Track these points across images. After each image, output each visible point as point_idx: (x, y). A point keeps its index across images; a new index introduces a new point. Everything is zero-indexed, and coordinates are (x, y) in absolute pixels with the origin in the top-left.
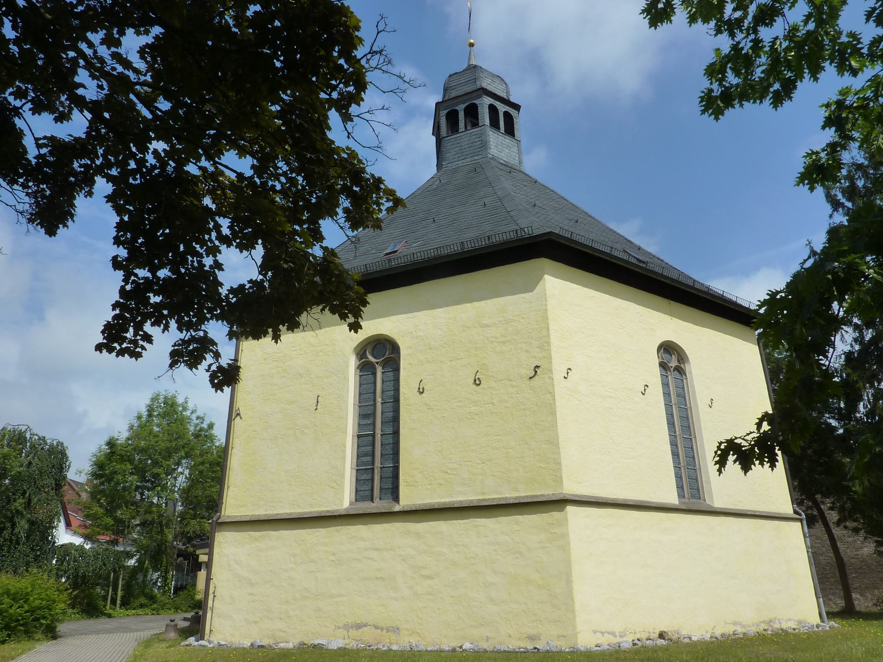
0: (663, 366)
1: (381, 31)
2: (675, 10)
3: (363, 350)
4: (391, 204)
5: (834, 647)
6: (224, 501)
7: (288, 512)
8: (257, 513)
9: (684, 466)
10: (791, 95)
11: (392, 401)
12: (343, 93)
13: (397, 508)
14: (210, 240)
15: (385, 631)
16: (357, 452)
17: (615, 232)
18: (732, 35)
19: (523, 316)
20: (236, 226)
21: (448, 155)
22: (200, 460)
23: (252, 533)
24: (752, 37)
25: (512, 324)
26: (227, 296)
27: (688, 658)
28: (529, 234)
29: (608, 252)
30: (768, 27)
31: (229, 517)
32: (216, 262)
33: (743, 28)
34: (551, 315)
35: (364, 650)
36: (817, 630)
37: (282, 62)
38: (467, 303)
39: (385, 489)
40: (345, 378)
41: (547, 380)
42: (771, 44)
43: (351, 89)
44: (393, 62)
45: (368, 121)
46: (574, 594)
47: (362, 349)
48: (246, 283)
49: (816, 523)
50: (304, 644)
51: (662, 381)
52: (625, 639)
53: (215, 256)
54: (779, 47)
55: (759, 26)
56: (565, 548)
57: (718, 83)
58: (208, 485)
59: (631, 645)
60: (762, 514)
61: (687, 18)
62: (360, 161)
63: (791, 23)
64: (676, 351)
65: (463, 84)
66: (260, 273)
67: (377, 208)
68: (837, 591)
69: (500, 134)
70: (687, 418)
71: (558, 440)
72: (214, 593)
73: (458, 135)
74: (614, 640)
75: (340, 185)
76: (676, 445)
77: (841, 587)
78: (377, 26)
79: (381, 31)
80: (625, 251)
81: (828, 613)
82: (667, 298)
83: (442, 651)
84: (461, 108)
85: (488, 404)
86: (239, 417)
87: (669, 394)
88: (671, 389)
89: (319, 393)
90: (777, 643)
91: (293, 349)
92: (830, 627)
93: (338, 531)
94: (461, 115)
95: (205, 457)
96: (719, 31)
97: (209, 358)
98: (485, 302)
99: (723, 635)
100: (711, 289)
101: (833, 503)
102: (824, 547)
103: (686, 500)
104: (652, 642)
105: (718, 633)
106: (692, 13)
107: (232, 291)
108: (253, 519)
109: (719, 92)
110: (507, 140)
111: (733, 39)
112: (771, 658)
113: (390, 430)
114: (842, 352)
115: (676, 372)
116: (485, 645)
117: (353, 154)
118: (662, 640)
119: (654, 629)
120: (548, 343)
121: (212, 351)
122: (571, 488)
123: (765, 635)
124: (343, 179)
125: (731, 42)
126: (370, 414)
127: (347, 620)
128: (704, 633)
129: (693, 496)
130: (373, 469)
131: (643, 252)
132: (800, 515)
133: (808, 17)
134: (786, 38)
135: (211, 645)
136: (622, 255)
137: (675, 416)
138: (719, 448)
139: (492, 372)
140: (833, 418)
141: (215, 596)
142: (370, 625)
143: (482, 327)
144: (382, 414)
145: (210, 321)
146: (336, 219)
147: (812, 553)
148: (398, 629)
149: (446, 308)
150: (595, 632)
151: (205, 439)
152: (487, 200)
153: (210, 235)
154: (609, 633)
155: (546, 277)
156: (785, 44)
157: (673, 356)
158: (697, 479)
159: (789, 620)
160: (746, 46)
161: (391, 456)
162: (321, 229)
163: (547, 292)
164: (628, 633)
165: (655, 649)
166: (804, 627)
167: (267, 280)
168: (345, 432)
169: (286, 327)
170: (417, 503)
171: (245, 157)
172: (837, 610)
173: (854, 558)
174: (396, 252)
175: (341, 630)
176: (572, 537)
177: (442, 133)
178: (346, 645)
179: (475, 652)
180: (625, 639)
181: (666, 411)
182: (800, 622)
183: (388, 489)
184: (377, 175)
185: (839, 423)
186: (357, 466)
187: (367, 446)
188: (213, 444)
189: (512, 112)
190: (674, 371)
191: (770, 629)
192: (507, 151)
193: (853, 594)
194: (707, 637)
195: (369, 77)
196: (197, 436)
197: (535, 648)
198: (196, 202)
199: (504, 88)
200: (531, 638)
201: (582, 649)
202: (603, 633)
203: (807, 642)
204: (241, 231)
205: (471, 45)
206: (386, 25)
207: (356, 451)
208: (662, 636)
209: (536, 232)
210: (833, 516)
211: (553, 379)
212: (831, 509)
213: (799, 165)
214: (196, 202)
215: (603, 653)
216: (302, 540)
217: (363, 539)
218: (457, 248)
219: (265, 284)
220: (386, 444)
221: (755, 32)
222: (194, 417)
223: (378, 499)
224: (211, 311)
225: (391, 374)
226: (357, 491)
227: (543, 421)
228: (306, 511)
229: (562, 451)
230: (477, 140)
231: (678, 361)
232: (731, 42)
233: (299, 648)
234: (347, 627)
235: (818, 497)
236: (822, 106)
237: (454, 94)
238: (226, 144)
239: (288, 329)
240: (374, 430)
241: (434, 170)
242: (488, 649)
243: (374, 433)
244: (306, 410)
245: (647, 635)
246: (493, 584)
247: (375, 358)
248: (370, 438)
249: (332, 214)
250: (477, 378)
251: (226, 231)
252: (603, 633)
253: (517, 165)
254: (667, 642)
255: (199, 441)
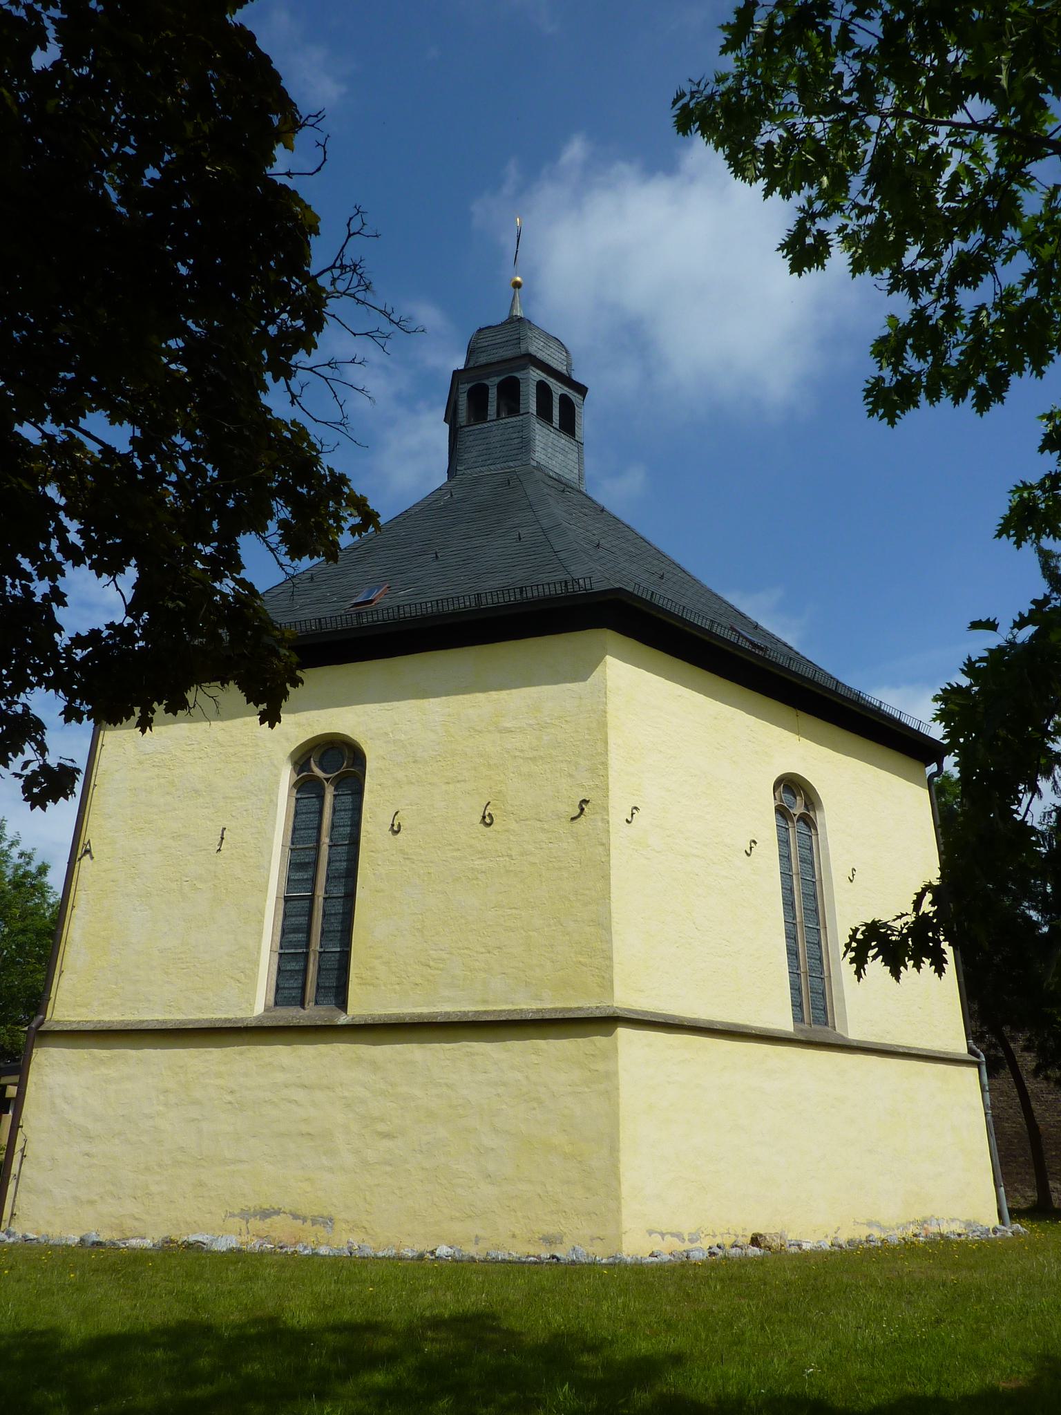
0: (782, 812)
1: (354, 234)
2: (831, 249)
3: (306, 759)
4: (358, 520)
5: (1018, 1262)
6: (52, 995)
7: (161, 1018)
8: (106, 1018)
9: (806, 972)
10: (1003, 394)
11: (346, 842)
12: (287, 328)
13: (343, 1020)
14: (47, 551)
15: (309, 1222)
16: (283, 925)
17: (720, 598)
18: (915, 295)
19: (568, 719)
20: (93, 531)
21: (466, 456)
22: (19, 925)
23: (97, 1052)
24: (946, 300)
25: (548, 730)
26: (68, 649)
27: (793, 1277)
28: (586, 590)
29: (707, 627)
30: (970, 288)
31: (58, 1022)
32: (55, 589)
33: (932, 286)
34: (611, 719)
35: (272, 1253)
36: (993, 1236)
37: (189, 267)
38: (479, 692)
39: (325, 988)
40: (271, 801)
41: (600, 824)
42: (974, 314)
43: (299, 323)
44: (374, 286)
45: (326, 379)
46: (621, 1170)
47: (303, 755)
48: (103, 628)
49: (1001, 1071)
50: (172, 1241)
51: (779, 836)
52: (697, 1245)
53: (54, 579)
54: (985, 319)
55: (958, 285)
56: (611, 1095)
57: (891, 367)
58: (31, 968)
59: (707, 1254)
60: (920, 1053)
61: (849, 264)
62: (312, 446)
63: (1005, 284)
64: (804, 791)
65: (502, 345)
66: (128, 613)
67: (335, 525)
68: (1027, 1177)
69: (552, 430)
70: (815, 896)
71: (610, 921)
72: (23, 1150)
73: (485, 425)
74: (680, 1247)
75: (277, 481)
76: (795, 939)
77: (1033, 1171)
78: (348, 225)
79: (354, 234)
80: (733, 629)
81: (1011, 1211)
82: (794, 707)
83: (401, 1258)
84: (493, 382)
85: (503, 856)
86: (88, 856)
87: (789, 858)
88: (792, 850)
89: (225, 823)
90: (932, 1256)
91: (189, 748)
92: (1013, 1233)
93: (241, 1053)
94: (493, 394)
95: (28, 922)
96: (894, 288)
97: (29, 752)
98: (508, 692)
99: (850, 1242)
100: (862, 698)
101: (1029, 1040)
102: (1011, 1108)
103: (806, 1026)
104: (739, 1250)
105: (843, 1239)
106: (857, 255)
107: (78, 641)
108: (99, 1027)
109: (893, 383)
110: (563, 441)
111: (915, 301)
112: (920, 1280)
113: (339, 891)
114: (1053, 808)
115: (802, 824)
116: (472, 1250)
117: (301, 433)
118: (755, 1248)
119: (744, 1229)
120: (605, 765)
121: (34, 739)
122: (625, 999)
123: (914, 1244)
124: (283, 473)
125: (913, 306)
126: (309, 863)
127: (246, 1203)
128: (821, 1237)
129: (816, 1020)
130: (307, 955)
131: (761, 632)
132: (978, 1056)
133: (1029, 277)
134: (996, 306)
135: (11, 1240)
136: (728, 635)
137: (796, 892)
138: (852, 938)
139: (512, 806)
140: (1035, 908)
141: (23, 1156)
142: (284, 1213)
143: (500, 732)
144: (329, 863)
145: (36, 688)
146: (263, 535)
147: (993, 1116)
148: (331, 1220)
149: (444, 698)
150: (650, 1232)
151: (32, 890)
152: (523, 531)
153: (49, 544)
154: (673, 1235)
155: (609, 659)
156: (994, 317)
157: (798, 798)
158: (823, 994)
159: (953, 1220)
160: (936, 314)
161: (339, 934)
162: (239, 552)
163: (609, 683)
164: (703, 1236)
165: (744, 1262)
166: (974, 1231)
167: (139, 625)
168: (264, 890)
169: (163, 707)
170: (376, 1012)
171: (121, 424)
172: (1025, 1206)
173: (1055, 1127)
174: (371, 601)
175: (237, 1219)
176: (624, 1078)
177: (460, 420)
178: (242, 1244)
179: (457, 1261)
180: (697, 1245)
181: (782, 884)
182: (968, 1224)
183: (329, 987)
184: (338, 470)
185: (1042, 917)
186: (281, 948)
187: (300, 916)
188: (45, 901)
189: (574, 396)
190: (798, 821)
191: (923, 1235)
192: (561, 457)
193: (1050, 1182)
194: (826, 1245)
195: (332, 306)
196: (17, 884)
197: (554, 1257)
198: (26, 486)
199: (563, 357)
200: (549, 1240)
201: (629, 1259)
202: (663, 1235)
203: (977, 1254)
204: (102, 540)
205: (517, 285)
206: (364, 224)
207: (280, 923)
208: (755, 1241)
209: (598, 587)
210: (1028, 1061)
211: (608, 822)
212: (1026, 1049)
213: (1002, 507)
214: (26, 486)
215: (660, 1267)
216: (181, 1067)
217: (283, 1069)
218: (469, 603)
219: (136, 632)
220: (331, 914)
221: (952, 293)
222: (15, 852)
223: (312, 1004)
224: (37, 671)
225: (348, 799)
226: (278, 988)
227: (589, 889)
228: (191, 1017)
229: (615, 937)
230: (515, 435)
231: (806, 806)
232: (913, 306)
233: (162, 1248)
234: (245, 1215)
235: (1006, 1030)
236: (1042, 417)
237: (483, 359)
238: (92, 400)
239: (167, 711)
240: (313, 890)
241: (444, 479)
242: (477, 1257)
243: (313, 895)
244: (201, 851)
245: (733, 1239)
246: (492, 1149)
247: (324, 771)
248: (306, 903)
249: (260, 528)
250: (487, 813)
251: (74, 538)
252: (663, 1235)
253: (575, 481)
254: (763, 1251)
255: (20, 893)
